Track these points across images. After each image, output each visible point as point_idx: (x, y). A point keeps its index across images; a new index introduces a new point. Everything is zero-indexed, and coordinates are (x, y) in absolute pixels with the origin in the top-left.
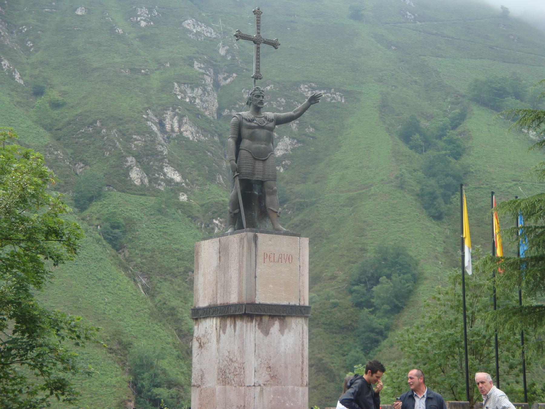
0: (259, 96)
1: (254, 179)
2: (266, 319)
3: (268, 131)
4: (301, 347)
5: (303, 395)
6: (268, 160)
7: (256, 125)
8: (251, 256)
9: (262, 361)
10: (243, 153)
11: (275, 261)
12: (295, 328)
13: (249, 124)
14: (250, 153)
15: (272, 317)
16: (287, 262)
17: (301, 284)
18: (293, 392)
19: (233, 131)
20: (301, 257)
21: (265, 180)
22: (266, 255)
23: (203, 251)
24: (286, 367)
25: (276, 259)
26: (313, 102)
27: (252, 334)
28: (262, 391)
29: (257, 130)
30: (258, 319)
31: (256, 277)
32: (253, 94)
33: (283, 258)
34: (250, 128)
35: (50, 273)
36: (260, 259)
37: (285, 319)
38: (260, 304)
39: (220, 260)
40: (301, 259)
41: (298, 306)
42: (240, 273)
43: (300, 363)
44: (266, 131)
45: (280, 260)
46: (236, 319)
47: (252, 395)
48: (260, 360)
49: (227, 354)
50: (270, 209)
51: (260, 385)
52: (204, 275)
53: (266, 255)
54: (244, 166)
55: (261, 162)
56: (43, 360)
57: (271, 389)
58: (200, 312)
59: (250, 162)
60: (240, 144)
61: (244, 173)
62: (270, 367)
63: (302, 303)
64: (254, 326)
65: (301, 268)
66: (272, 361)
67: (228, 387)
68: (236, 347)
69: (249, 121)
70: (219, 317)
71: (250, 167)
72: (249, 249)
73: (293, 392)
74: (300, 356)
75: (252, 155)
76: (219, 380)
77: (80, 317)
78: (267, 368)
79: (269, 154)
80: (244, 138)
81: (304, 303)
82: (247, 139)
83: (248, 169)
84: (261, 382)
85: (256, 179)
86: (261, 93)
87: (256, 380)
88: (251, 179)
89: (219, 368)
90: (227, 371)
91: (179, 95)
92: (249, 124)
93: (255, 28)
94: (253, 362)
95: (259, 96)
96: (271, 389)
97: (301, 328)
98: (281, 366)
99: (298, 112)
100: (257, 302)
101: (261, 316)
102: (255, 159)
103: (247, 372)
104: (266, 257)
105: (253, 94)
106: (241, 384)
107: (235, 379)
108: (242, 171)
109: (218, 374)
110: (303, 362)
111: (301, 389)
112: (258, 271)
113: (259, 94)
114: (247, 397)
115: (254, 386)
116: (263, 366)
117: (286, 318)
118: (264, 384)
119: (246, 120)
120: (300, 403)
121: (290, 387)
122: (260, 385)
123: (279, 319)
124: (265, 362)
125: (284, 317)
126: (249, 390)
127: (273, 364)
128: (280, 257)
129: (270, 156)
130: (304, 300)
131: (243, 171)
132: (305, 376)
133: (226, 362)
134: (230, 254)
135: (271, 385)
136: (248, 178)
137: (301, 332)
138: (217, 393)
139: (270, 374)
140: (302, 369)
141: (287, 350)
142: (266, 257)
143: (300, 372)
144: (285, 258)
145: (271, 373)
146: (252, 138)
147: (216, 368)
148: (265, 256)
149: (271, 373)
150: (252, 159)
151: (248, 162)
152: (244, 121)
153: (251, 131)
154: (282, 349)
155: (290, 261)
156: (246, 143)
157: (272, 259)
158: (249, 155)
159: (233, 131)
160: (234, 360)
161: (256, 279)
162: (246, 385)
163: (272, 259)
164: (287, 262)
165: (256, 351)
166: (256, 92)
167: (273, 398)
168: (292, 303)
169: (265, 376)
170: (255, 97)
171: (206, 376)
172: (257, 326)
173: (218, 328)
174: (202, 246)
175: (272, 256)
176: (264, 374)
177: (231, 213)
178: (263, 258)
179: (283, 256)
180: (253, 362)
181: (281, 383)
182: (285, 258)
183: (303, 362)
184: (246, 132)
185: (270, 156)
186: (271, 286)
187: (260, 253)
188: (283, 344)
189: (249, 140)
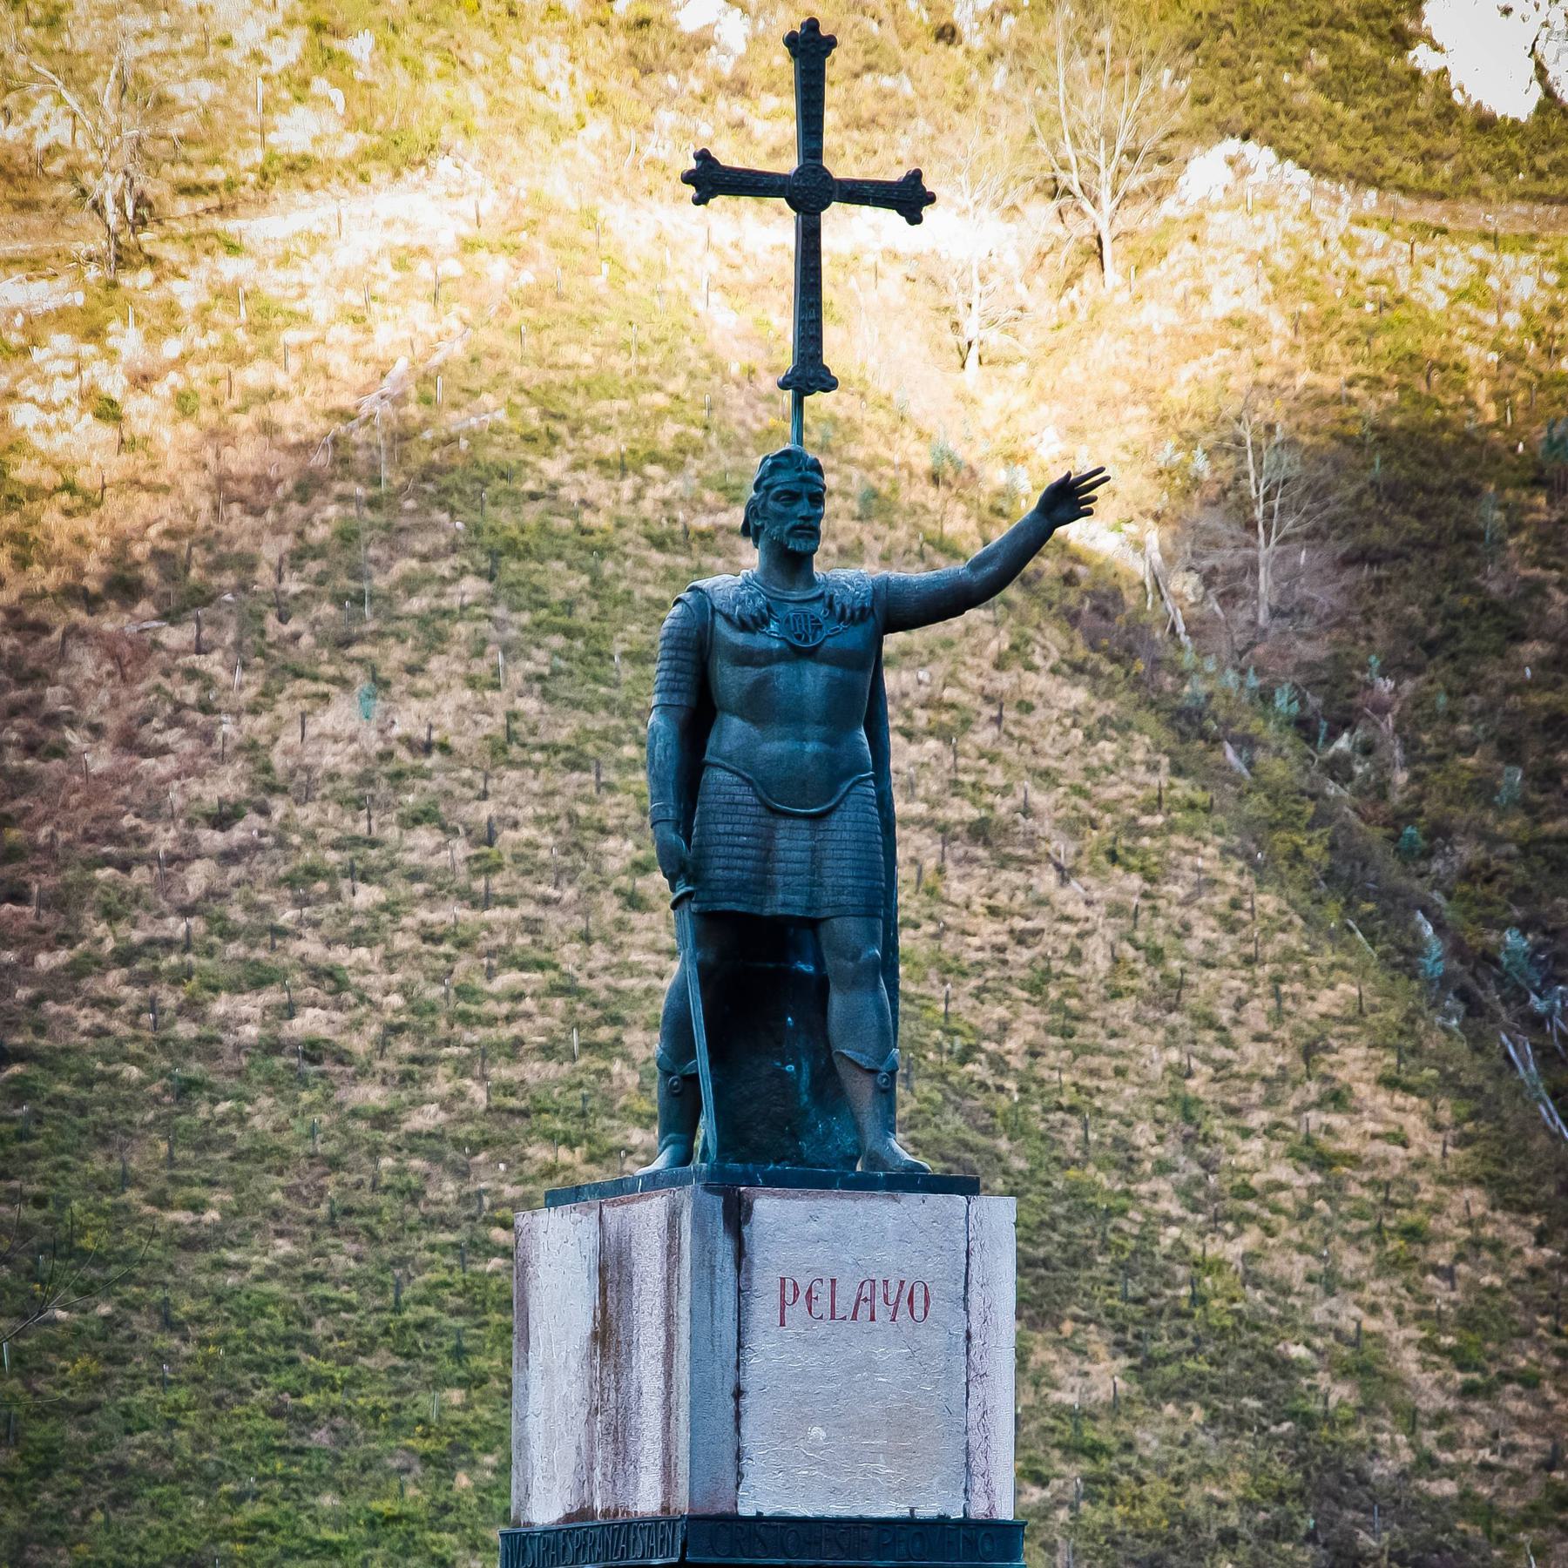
0: (793, 497)
1: (767, 911)
3: (838, 672)
6: (836, 817)
7: (776, 645)
8: (712, 1294)
10: (717, 778)
11: (839, 1314)
13: (739, 638)
14: (749, 782)
16: (903, 1315)
17: (974, 1416)
19: (671, 675)
20: (974, 1287)
22: (789, 1291)
23: (542, 1258)
25: (844, 1305)
26: (1060, 513)
29: (780, 668)
31: (738, 1394)
32: (769, 488)
33: (879, 1300)
34: (745, 658)
36: (763, 1310)
38: (759, 1518)
40: (975, 1300)
41: (959, 1523)
42: (668, 1375)
44: (824, 669)
45: (864, 1309)
53: (789, 1291)
54: (721, 850)
55: (804, 824)
56: (92, 447)
59: (748, 829)
61: (721, 885)
63: (979, 1510)
65: (976, 1341)
72: (705, 1265)
75: (757, 795)
79: (845, 787)
80: (724, 710)
81: (992, 1508)
82: (734, 714)
83: (739, 863)
85: (780, 911)
86: (804, 480)
88: (756, 910)
91: (1141, 731)
92: (739, 638)
93: (788, 129)
95: (793, 497)
100: (746, 1510)
104: (789, 1297)
105: (769, 488)
113: (792, 487)
119: (728, 618)
128: (866, 1292)
129: (847, 793)
130: (989, 1494)
131: (716, 872)
142: (789, 1297)
144: (892, 1299)
146: (758, 707)
148: (789, 1292)
150: (761, 810)
151: (738, 828)
152: (721, 625)
153: (751, 674)
155: (919, 1313)
156: (732, 732)
158: (744, 795)
159: (671, 675)
161: (745, 1402)
164: (903, 1315)
170: (776, 498)
174: (541, 1234)
177: (667, 1074)
178: (777, 1301)
179: (880, 1289)
182: (892, 1299)
184: (731, 679)
185: (847, 793)
186: (817, 1432)
187: (765, 1280)
189: (742, 717)
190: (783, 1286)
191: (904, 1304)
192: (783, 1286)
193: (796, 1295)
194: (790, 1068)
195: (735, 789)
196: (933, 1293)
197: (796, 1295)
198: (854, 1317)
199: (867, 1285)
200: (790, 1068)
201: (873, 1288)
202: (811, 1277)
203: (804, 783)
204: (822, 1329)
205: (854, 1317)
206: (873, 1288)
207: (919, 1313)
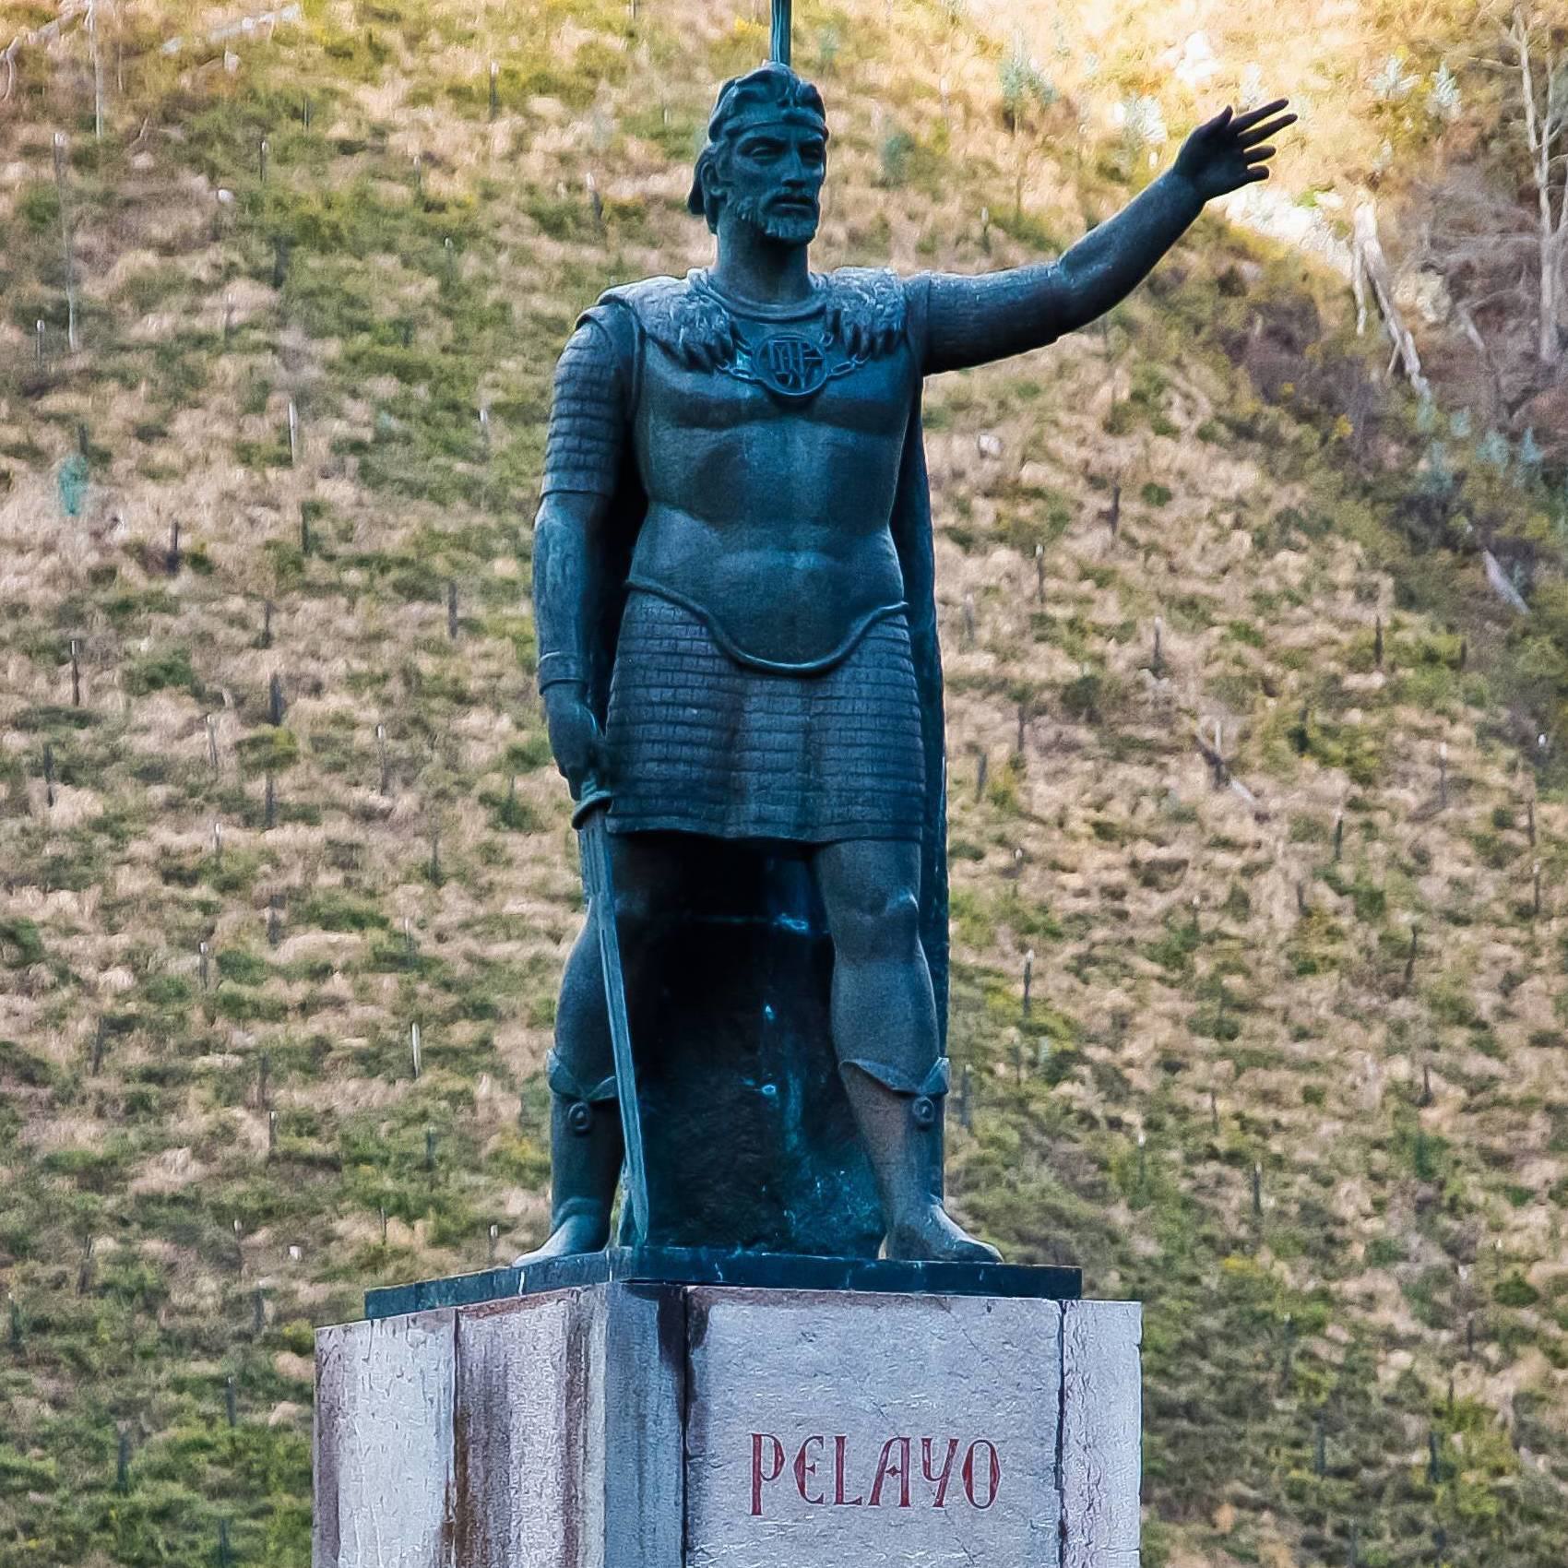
0: (774, 148)
1: (732, 832)
6: (844, 675)
7: (747, 392)
8: (641, 1462)
11: (850, 1495)
13: (685, 382)
14: (701, 619)
19: (572, 442)
20: (1072, 1452)
25: (858, 1480)
26: (1214, 175)
29: (752, 431)
32: (733, 134)
33: (915, 1472)
39: (685, 1425)
40: (1072, 1468)
44: (825, 433)
45: (891, 1486)
50: (856, 1067)
54: (655, 731)
55: (791, 687)
59: (700, 695)
61: (656, 788)
65: (1076, 1539)
71: (702, 733)
79: (859, 626)
82: (676, 506)
83: (686, 751)
85: (753, 831)
86: (792, 120)
88: (713, 830)
92: (685, 382)
95: (774, 148)
99: (1098, 268)
102: (744, 668)
104: (768, 1467)
105: (733, 134)
108: (637, 771)
119: (667, 349)
128: (895, 1458)
134: (514, 1437)
136: (688, 826)
142: (768, 1467)
144: (937, 1470)
150: (721, 665)
151: (683, 694)
152: (655, 361)
153: (704, 441)
155: (981, 1493)
157: (820, 1484)
158: (694, 640)
159: (572, 442)
163: (820, 1484)
170: (746, 151)
174: (358, 1362)
177: (566, 1099)
178: (747, 1473)
179: (917, 1454)
182: (937, 1470)
189: (690, 511)
190: (757, 1450)
191: (957, 1478)
192: (757, 1450)
193: (779, 1464)
194: (769, 1089)
195: (678, 630)
196: (1005, 1460)
197: (779, 1464)
198: (875, 1500)
199: (896, 1448)
200: (769, 1089)
201: (906, 1452)
202: (804, 1432)
203: (792, 621)
204: (821, 1518)
205: (875, 1500)
206: (906, 1452)
207: (981, 1493)
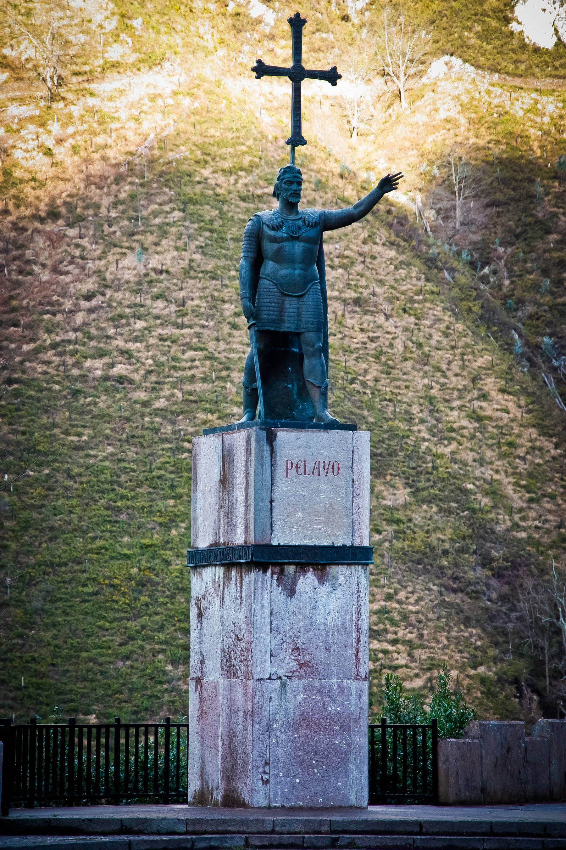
1: (282, 330)
2: (290, 570)
3: (307, 245)
4: (355, 615)
5: (360, 693)
6: (306, 296)
7: (285, 235)
9: (285, 638)
10: (264, 283)
12: (343, 583)
13: (272, 233)
14: (275, 284)
15: (303, 567)
17: (355, 509)
18: (341, 689)
20: (355, 464)
21: (303, 330)
24: (328, 649)
25: (309, 470)
27: (265, 596)
28: (283, 686)
29: (286, 244)
30: (277, 569)
31: (272, 501)
33: (321, 468)
35: (168, 380)
36: (280, 472)
37: (325, 569)
41: (350, 547)
42: (247, 495)
43: (354, 641)
44: (302, 244)
45: (316, 471)
46: (243, 571)
47: (267, 693)
48: (280, 636)
49: (232, 627)
51: (280, 678)
52: (204, 494)
55: (295, 299)
57: (301, 684)
58: (199, 557)
60: (260, 267)
62: (298, 649)
63: (357, 543)
64: (269, 581)
65: (356, 483)
66: (301, 638)
67: (233, 680)
68: (243, 617)
69: (273, 229)
70: (222, 565)
72: (260, 455)
73: (341, 689)
74: (354, 630)
76: (222, 669)
77: (511, 406)
78: (293, 650)
79: (309, 286)
81: (361, 542)
84: (282, 672)
86: (295, 177)
87: (274, 669)
89: (223, 651)
90: (232, 655)
92: (272, 233)
94: (268, 641)
95: (291, 183)
96: (301, 684)
97: (355, 585)
98: (318, 647)
99: (361, 208)
100: (274, 543)
101: (282, 564)
103: (257, 656)
104: (290, 467)
106: (248, 675)
107: (242, 668)
109: (222, 660)
110: (358, 640)
111: (354, 684)
112: (278, 491)
114: (257, 697)
115: (270, 679)
116: (286, 647)
117: (328, 568)
118: (288, 677)
120: (353, 708)
121: (335, 681)
122: (280, 678)
123: (314, 569)
124: (290, 641)
125: (324, 565)
126: (261, 685)
127: (303, 644)
128: (317, 465)
130: (361, 537)
132: (363, 663)
133: (231, 640)
135: (300, 677)
137: (355, 591)
138: (221, 691)
139: (297, 660)
140: (358, 652)
141: (330, 620)
142: (290, 467)
143: (354, 657)
145: (300, 658)
146: (279, 257)
147: (219, 650)
149: (300, 658)
153: (276, 246)
154: (321, 619)
155: (336, 473)
156: (269, 266)
157: (301, 470)
160: (241, 636)
162: (256, 677)
163: (301, 470)
165: (274, 623)
166: (287, 176)
167: (304, 699)
168: (339, 543)
169: (288, 663)
171: (207, 662)
172: (275, 582)
173: (221, 583)
175: (302, 465)
176: (287, 660)
177: (246, 388)
179: (322, 464)
180: (268, 641)
181: (319, 674)
183: (358, 640)
184: (269, 247)
186: (300, 515)
187: (281, 461)
188: (322, 611)
189: (273, 261)
